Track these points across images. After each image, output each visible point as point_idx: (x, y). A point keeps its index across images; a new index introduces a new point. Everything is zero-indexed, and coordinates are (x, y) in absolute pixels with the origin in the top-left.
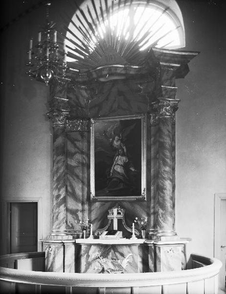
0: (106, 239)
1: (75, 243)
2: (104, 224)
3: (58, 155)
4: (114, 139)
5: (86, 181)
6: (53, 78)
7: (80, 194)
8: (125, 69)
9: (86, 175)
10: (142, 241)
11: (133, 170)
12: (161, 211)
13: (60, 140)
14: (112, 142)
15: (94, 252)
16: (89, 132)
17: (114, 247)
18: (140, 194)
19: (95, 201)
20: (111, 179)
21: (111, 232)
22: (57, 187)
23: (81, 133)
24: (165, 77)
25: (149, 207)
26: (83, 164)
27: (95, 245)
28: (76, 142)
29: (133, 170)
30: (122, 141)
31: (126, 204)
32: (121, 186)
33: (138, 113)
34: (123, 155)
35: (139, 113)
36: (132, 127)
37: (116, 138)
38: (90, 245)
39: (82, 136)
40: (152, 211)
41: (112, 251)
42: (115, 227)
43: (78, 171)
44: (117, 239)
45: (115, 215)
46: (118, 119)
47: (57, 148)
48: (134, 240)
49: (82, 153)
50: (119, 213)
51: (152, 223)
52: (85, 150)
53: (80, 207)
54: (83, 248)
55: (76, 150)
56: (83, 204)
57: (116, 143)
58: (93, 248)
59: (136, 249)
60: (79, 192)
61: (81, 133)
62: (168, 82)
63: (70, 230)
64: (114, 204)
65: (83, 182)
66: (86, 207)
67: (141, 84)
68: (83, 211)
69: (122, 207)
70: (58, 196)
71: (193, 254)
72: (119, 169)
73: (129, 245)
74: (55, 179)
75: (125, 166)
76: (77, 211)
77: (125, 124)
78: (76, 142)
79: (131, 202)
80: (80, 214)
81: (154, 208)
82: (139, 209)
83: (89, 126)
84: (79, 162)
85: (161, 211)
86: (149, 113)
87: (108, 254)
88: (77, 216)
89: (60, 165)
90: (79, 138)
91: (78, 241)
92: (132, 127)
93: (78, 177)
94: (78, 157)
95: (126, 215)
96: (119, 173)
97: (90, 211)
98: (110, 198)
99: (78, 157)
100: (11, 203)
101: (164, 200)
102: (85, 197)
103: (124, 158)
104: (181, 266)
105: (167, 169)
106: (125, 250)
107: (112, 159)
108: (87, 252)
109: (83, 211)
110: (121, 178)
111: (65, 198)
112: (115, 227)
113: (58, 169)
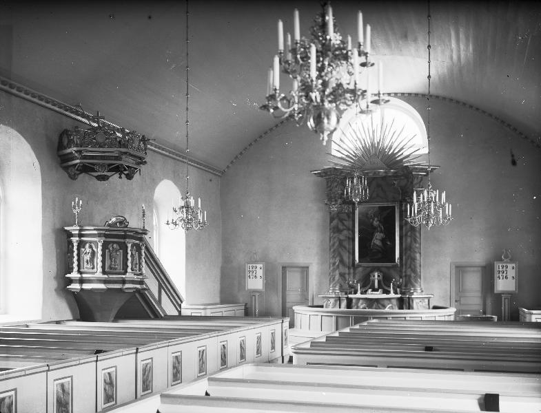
0: (371, 295)
1: (347, 298)
2: (367, 284)
3: (334, 233)
4: (374, 220)
5: (351, 251)
6: (269, 111)
7: (347, 261)
8: (385, 172)
9: (351, 247)
10: (399, 296)
11: (389, 243)
12: (413, 275)
13: (335, 222)
14: (373, 222)
15: (362, 304)
16: (354, 213)
17: (377, 300)
18: (395, 262)
19: (359, 266)
20: (372, 250)
21: (374, 290)
22: (333, 256)
23: (348, 215)
24: (415, 181)
25: (401, 271)
26: (349, 238)
27: (362, 299)
28: (344, 222)
29: (389, 243)
30: (380, 221)
31: (383, 269)
32: (380, 255)
33: (393, 201)
34: (381, 232)
35: (394, 201)
36: (388, 211)
37: (376, 219)
38: (359, 299)
39: (349, 217)
40: (404, 274)
41: (376, 303)
42: (376, 285)
43: (346, 244)
44: (379, 295)
45: (376, 276)
46: (377, 205)
47: (334, 228)
48: (392, 295)
49: (349, 229)
50: (379, 276)
51: (404, 283)
52: (351, 227)
53: (347, 271)
54: (354, 301)
55: (345, 228)
56: (349, 268)
57: (376, 223)
58: (361, 301)
59: (394, 302)
60: (346, 259)
61: (348, 215)
62: (418, 185)
63: (341, 289)
64: (373, 270)
65: (349, 252)
66: (352, 271)
67: (395, 180)
68: (349, 274)
69: (381, 272)
70: (334, 264)
71: (488, 393)
72: (378, 243)
73: (389, 299)
74: (332, 250)
75: (383, 240)
76: (345, 274)
77: (382, 209)
78: (344, 222)
79: (386, 267)
80: (347, 276)
81: (405, 272)
82: (393, 273)
83: (354, 210)
84: (346, 237)
85: (413, 275)
86: (401, 202)
87: (372, 306)
88: (345, 278)
89: (335, 240)
90: (346, 218)
91: (350, 296)
92: (388, 211)
93: (345, 248)
94: (345, 232)
95: (383, 277)
96: (377, 245)
97: (354, 274)
98: (371, 264)
99: (345, 232)
100: (284, 268)
101: (415, 267)
102: (351, 264)
103: (382, 235)
104: (360, 63)
105: (417, 245)
106: (386, 302)
107: (372, 235)
108: (357, 303)
109: (349, 274)
110: (380, 249)
111: (338, 265)
112: (376, 285)
113: (333, 245)
